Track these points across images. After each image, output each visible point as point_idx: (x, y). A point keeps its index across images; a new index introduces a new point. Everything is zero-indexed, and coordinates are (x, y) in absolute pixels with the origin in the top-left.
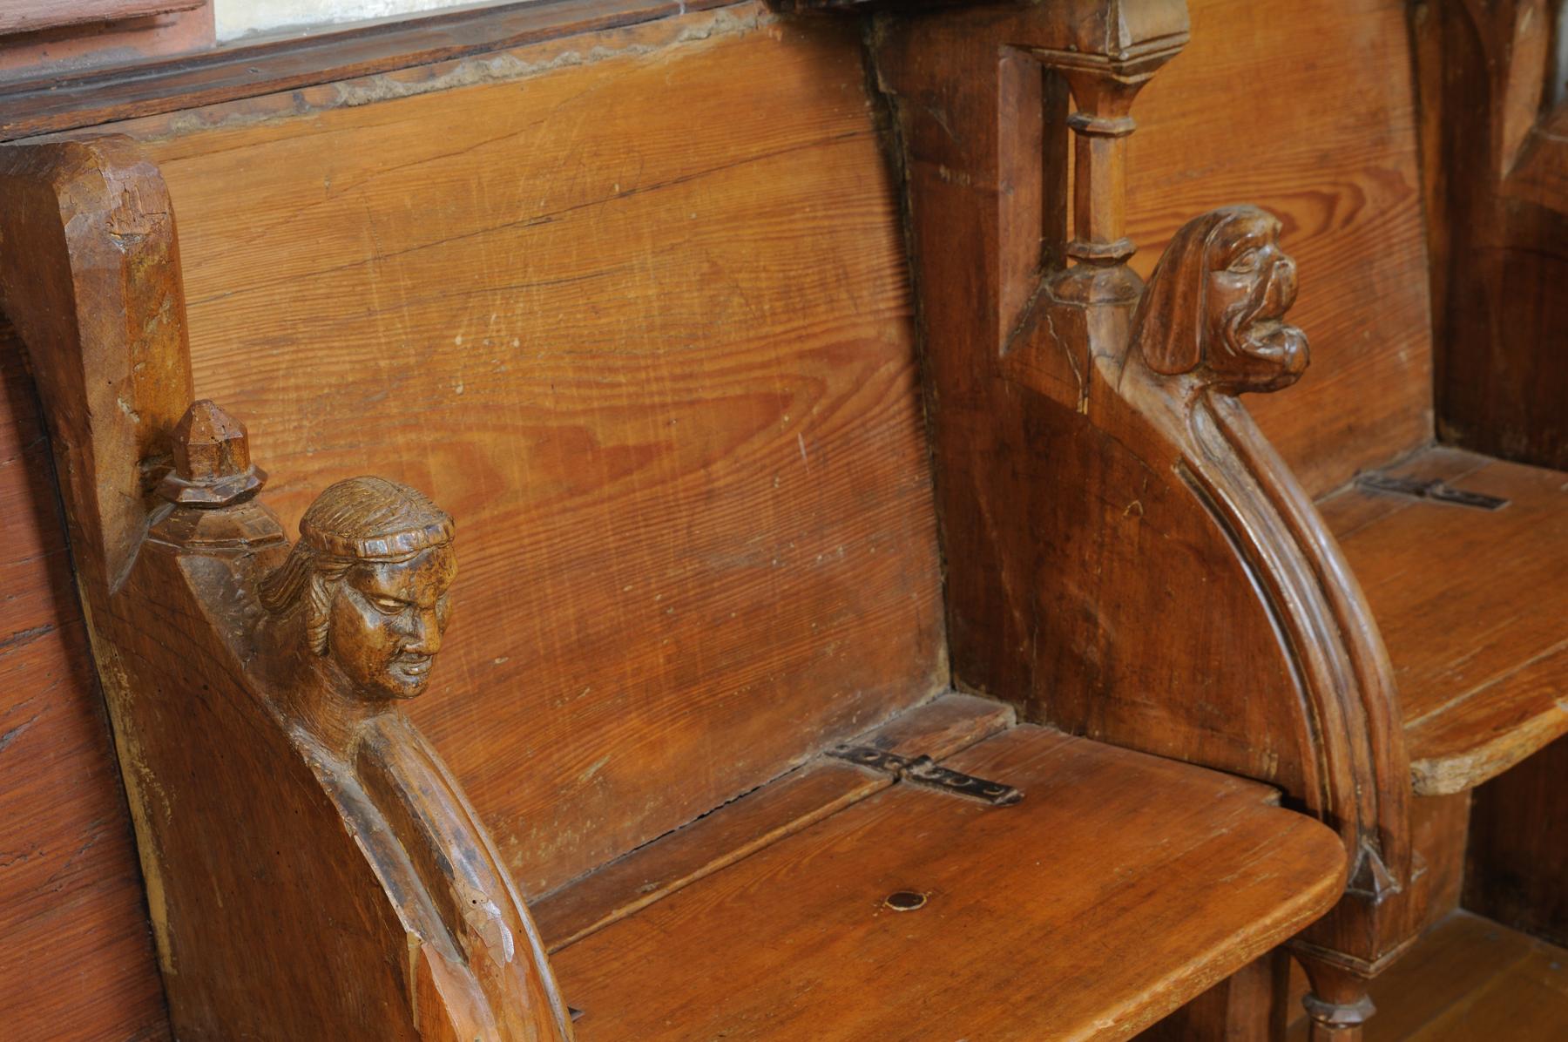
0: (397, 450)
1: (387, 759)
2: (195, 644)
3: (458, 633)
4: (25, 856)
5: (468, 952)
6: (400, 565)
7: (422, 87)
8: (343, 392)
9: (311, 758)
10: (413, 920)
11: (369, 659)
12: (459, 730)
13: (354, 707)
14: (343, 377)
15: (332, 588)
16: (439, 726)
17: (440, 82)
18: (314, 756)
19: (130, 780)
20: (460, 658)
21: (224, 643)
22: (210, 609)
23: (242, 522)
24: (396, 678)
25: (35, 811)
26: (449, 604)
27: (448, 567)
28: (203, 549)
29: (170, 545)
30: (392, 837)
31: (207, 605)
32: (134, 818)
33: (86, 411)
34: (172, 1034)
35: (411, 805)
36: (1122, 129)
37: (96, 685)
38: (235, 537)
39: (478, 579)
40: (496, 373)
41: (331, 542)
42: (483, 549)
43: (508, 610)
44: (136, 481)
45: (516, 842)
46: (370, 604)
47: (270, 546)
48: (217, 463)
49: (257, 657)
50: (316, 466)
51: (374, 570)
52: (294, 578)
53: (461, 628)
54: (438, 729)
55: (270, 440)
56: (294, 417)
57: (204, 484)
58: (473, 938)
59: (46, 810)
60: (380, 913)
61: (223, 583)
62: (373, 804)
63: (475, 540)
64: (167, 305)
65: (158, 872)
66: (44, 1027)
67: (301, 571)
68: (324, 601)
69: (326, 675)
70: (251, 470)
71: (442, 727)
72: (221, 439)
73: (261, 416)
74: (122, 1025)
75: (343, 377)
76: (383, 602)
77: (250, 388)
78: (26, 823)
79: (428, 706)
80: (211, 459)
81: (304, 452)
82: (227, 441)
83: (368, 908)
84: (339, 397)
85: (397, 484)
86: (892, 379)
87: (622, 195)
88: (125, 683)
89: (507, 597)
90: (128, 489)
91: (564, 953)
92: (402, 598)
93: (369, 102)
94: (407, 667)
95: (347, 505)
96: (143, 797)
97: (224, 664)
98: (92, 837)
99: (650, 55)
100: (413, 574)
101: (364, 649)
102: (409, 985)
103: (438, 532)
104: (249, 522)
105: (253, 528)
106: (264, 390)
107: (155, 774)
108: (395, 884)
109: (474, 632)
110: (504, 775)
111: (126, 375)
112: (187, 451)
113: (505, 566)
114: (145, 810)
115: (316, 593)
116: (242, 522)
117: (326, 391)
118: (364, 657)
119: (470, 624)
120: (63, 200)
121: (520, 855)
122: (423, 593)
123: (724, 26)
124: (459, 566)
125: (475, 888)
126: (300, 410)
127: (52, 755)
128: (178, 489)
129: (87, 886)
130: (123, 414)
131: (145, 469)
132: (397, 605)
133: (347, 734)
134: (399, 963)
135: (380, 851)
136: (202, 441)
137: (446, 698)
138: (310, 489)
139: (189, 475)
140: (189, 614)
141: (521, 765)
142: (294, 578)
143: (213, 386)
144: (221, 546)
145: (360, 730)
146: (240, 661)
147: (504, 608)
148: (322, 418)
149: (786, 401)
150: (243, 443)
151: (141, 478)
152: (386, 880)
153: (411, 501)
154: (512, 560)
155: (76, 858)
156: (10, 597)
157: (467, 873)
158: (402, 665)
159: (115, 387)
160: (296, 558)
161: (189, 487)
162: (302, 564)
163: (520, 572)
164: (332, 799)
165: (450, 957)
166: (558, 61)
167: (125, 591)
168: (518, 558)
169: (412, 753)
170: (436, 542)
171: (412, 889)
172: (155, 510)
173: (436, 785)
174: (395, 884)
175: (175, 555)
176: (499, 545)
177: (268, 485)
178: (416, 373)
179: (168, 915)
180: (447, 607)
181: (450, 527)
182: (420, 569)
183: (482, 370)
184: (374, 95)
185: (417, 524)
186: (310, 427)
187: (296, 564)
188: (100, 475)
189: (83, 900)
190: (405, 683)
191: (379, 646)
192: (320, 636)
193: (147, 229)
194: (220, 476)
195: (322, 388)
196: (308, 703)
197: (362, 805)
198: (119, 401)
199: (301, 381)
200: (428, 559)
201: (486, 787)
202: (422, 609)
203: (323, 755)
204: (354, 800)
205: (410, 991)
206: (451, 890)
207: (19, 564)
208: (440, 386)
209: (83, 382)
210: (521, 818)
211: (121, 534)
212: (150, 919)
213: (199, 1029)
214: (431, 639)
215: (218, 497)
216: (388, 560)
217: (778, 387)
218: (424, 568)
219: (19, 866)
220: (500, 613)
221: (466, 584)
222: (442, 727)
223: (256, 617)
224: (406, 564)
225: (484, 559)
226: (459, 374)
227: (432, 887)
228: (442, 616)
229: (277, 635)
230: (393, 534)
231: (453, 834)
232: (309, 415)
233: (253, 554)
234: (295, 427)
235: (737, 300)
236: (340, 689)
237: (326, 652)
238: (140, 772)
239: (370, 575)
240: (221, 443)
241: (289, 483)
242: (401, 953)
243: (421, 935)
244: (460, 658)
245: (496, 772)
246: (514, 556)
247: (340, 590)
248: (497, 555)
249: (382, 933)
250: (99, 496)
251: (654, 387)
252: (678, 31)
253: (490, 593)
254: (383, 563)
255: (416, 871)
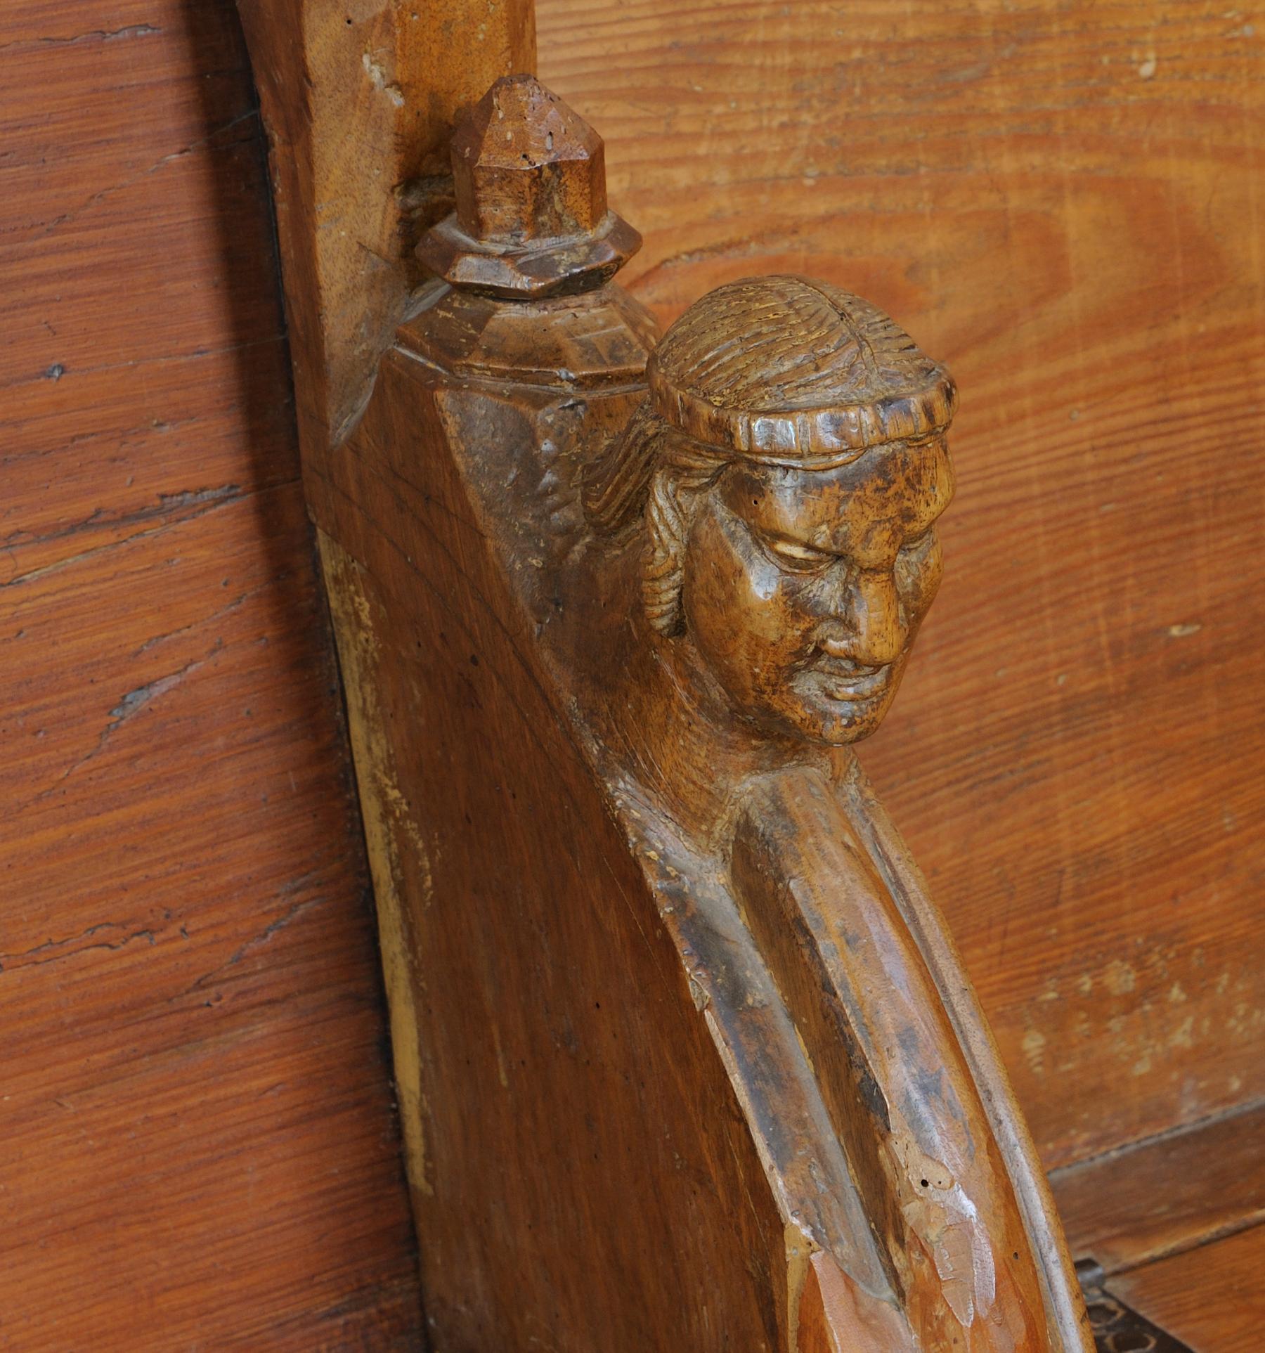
0: (997, 185)
1: (788, 863)
2: (459, 570)
3: (1096, 567)
4: (152, 932)
5: (907, 1280)
6: (820, 476)
8: (892, 58)
9: (642, 839)
10: (802, 1202)
11: (753, 658)
12: (1079, 763)
13: (730, 746)
14: (895, 30)
15: (692, 504)
16: (1034, 751)
18: (649, 834)
19: (371, 808)
20: (1094, 618)
21: (506, 579)
22: (488, 507)
23: (570, 335)
24: (808, 703)
25: (177, 849)
26: (932, 562)
27: (926, 487)
28: (487, 382)
29: (431, 365)
30: (783, 1022)
31: (483, 498)
32: (375, 879)
33: (303, 76)
34: (422, 1307)
35: (822, 966)
37: (320, 609)
38: (550, 365)
39: (1145, 462)
40: (1232, 40)
41: (689, 410)
42: (1166, 401)
43: (1207, 529)
44: (391, 226)
45: (1183, 997)
46: (760, 548)
47: (618, 389)
48: (530, 208)
49: (562, 616)
50: (820, 206)
51: (767, 480)
52: (629, 472)
53: (1103, 558)
54: (1034, 758)
55: (728, 148)
56: (781, 104)
57: (501, 249)
58: (915, 1256)
59: (200, 848)
60: (741, 1174)
61: (517, 455)
62: (757, 948)
63: (1148, 381)
65: (410, 994)
66: (165, 1264)
67: (643, 458)
68: (674, 528)
69: (679, 674)
70: (606, 225)
71: (1045, 754)
72: (541, 160)
73: (712, 97)
74: (325, 1277)
75: (895, 30)
76: (782, 547)
77: (693, 38)
78: (158, 870)
79: (1016, 710)
80: (519, 199)
81: (796, 177)
82: (553, 166)
83: (722, 1158)
84: (882, 69)
85: (842, 302)
88: (365, 617)
89: (1210, 502)
90: (376, 240)
91: (1239, 1244)
92: (819, 543)
94: (831, 685)
95: (730, 337)
96: (389, 844)
97: (504, 621)
98: (292, 907)
100: (848, 497)
101: (743, 639)
102: (785, 1329)
103: (908, 413)
104: (585, 336)
105: (589, 349)
106: (723, 45)
107: (409, 804)
108: (774, 1120)
109: (1131, 569)
110: (1168, 862)
111: (381, 9)
112: (474, 179)
113: (1209, 438)
114: (392, 870)
115: (660, 510)
116: (570, 335)
117: (857, 54)
118: (743, 654)
119: (1124, 551)
121: (1188, 1024)
122: (866, 538)
124: (954, 487)
125: (928, 1153)
126: (796, 91)
127: (220, 742)
128: (451, 253)
129: (271, 1002)
130: (372, 87)
131: (412, 201)
132: (810, 555)
133: (716, 799)
134: (769, 1279)
135: (754, 1048)
136: (503, 161)
137: (1055, 698)
138: (803, 254)
139: (477, 228)
140: (452, 510)
141: (1207, 845)
142: (629, 472)
143: (617, 29)
144: (525, 381)
145: (742, 794)
146: (531, 619)
147: (1200, 523)
148: (841, 109)
150: (594, 170)
151: (401, 221)
152: (757, 1111)
153: (861, 341)
154: (1228, 428)
155: (254, 946)
156: (160, 425)
157: (916, 1123)
158: (822, 677)
159: (359, 31)
160: (635, 430)
161: (471, 252)
162: (646, 444)
163: (1245, 453)
164: (673, 930)
165: (870, 1286)
167: (353, 443)
168: (1241, 424)
169: (839, 856)
170: (902, 434)
171: (809, 1137)
172: (426, 286)
173: (880, 928)
174: (774, 1120)
175: (434, 388)
176: (1201, 394)
177: (637, 265)
178: (1055, 29)
179: (422, 1079)
180: (927, 567)
181: (940, 405)
182: (862, 487)
183: (1200, 31)
185: (865, 392)
186: (816, 127)
187: (634, 443)
188: (324, 206)
189: (261, 1029)
190: (825, 715)
191: (773, 636)
192: (664, 598)
194: (536, 235)
195: (848, 48)
196: (644, 726)
197: (733, 948)
198: (366, 59)
199: (805, 31)
200: (883, 468)
201: (1125, 884)
202: (863, 571)
203: (666, 834)
204: (717, 935)
205: (785, 1340)
206: (882, 1152)
207: (183, 360)
208: (1106, 60)
209: (299, 14)
210: (1197, 951)
211: (357, 326)
212: (393, 1079)
213: (463, 1309)
214: (878, 634)
215: (525, 279)
216: (794, 463)
218: (870, 487)
219: (137, 950)
220: (1190, 533)
221: (1123, 469)
222: (1045, 754)
223: (570, 533)
224: (833, 474)
225: (1166, 420)
226: (1149, 37)
227: (848, 1136)
228: (915, 585)
229: (602, 577)
230: (810, 409)
231: (898, 1035)
232: (815, 103)
233: (581, 402)
234: (783, 126)
236: (705, 705)
237: (679, 629)
238: (386, 794)
240: (540, 169)
241: (759, 237)
242: (774, 1262)
243: (814, 1232)
244: (1094, 618)
245: (1150, 853)
246: (1232, 420)
247: (706, 511)
248: (1196, 415)
249: (743, 1215)
250: (320, 247)
253: (1173, 490)
254: (786, 469)
255: (824, 1098)
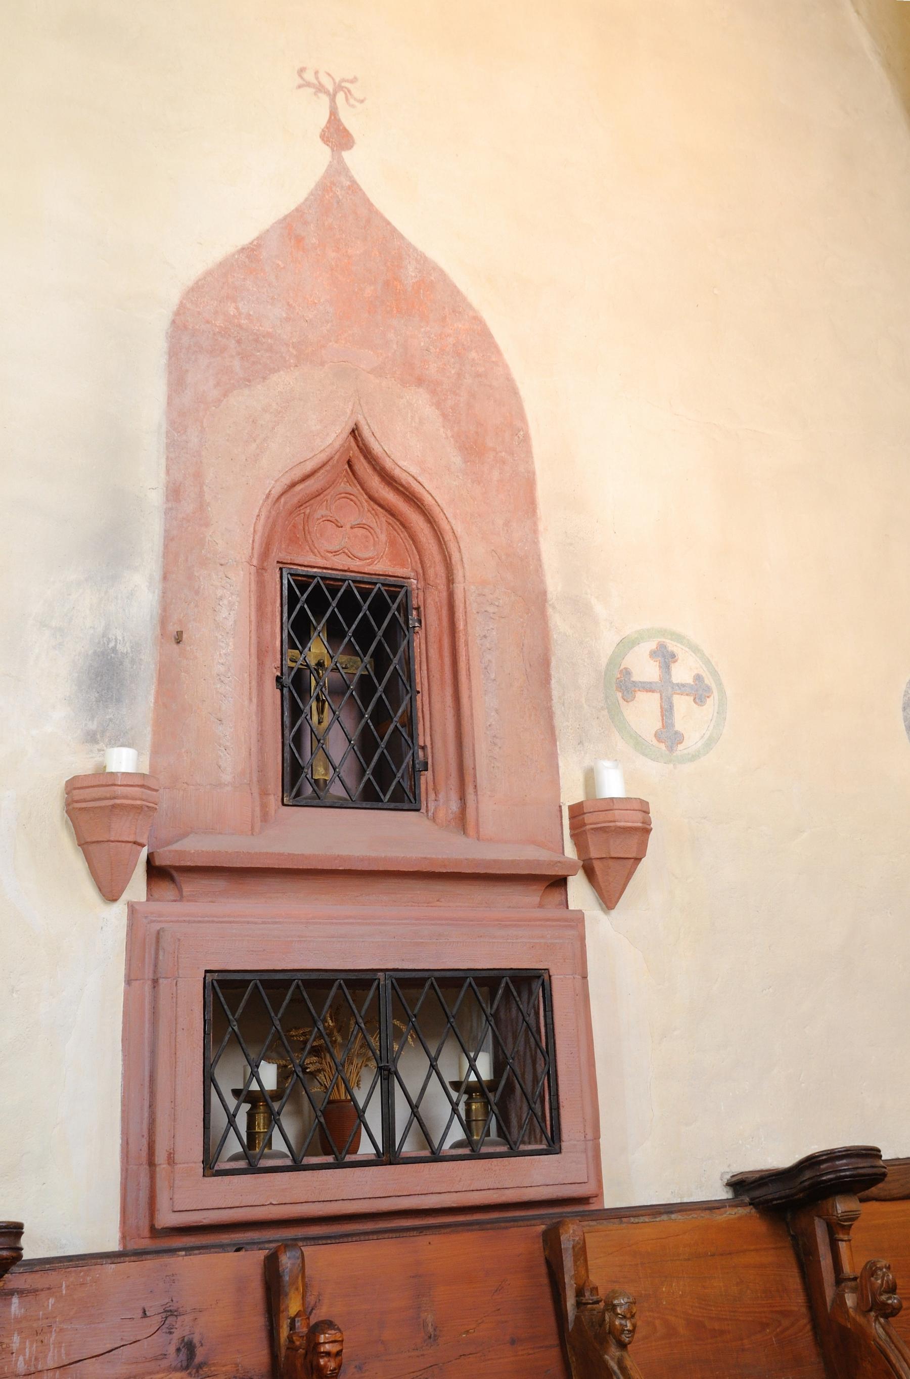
7: (653, 1220)
17: (657, 1219)
33: (565, 1283)
36: (846, 1239)
64: (582, 1258)
86: (805, 1325)
87: (711, 1255)
93: (638, 1223)
99: (717, 1217)
120: (561, 1231)
123: (740, 1212)
149: (768, 1325)
166: (690, 1217)
184: (640, 1221)
193: (577, 1239)
217: (764, 1320)
235: (749, 1291)
239: (616, 1309)
251: (723, 1313)
252: (726, 1212)
